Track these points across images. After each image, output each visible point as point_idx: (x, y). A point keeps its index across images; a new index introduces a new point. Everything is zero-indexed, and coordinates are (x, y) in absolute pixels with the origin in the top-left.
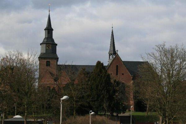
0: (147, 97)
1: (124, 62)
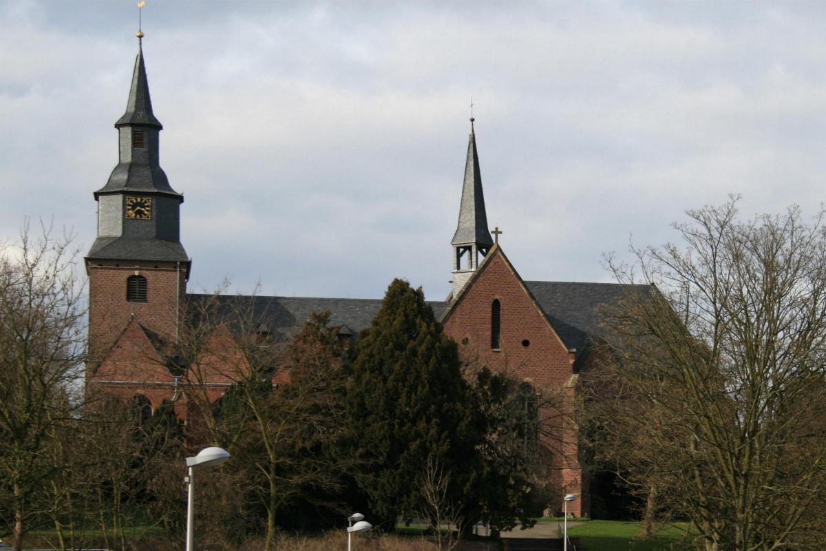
0: (640, 455)
1: (538, 291)
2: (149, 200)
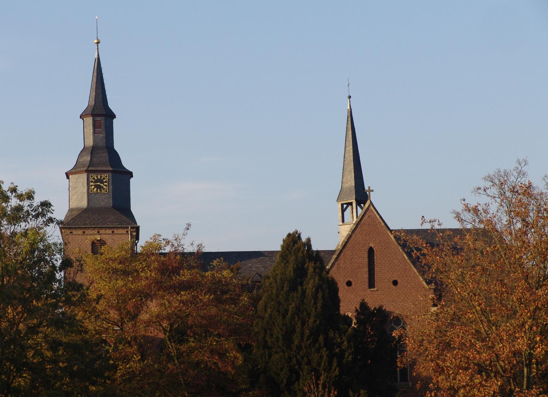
2: (106, 176)
